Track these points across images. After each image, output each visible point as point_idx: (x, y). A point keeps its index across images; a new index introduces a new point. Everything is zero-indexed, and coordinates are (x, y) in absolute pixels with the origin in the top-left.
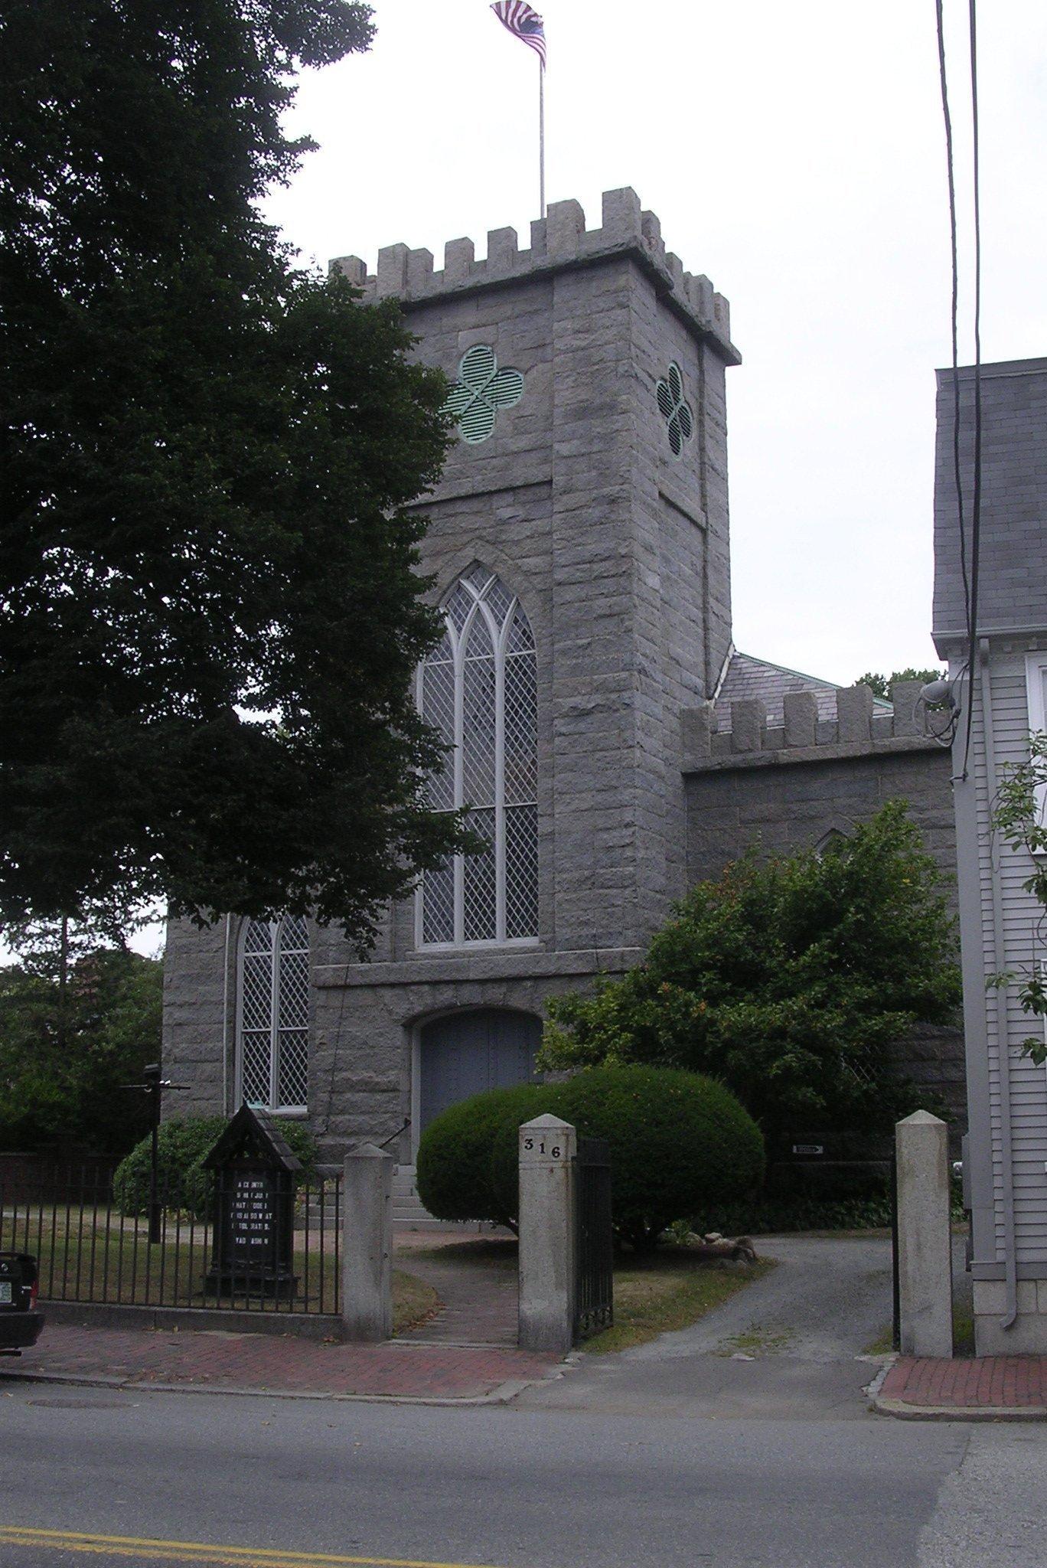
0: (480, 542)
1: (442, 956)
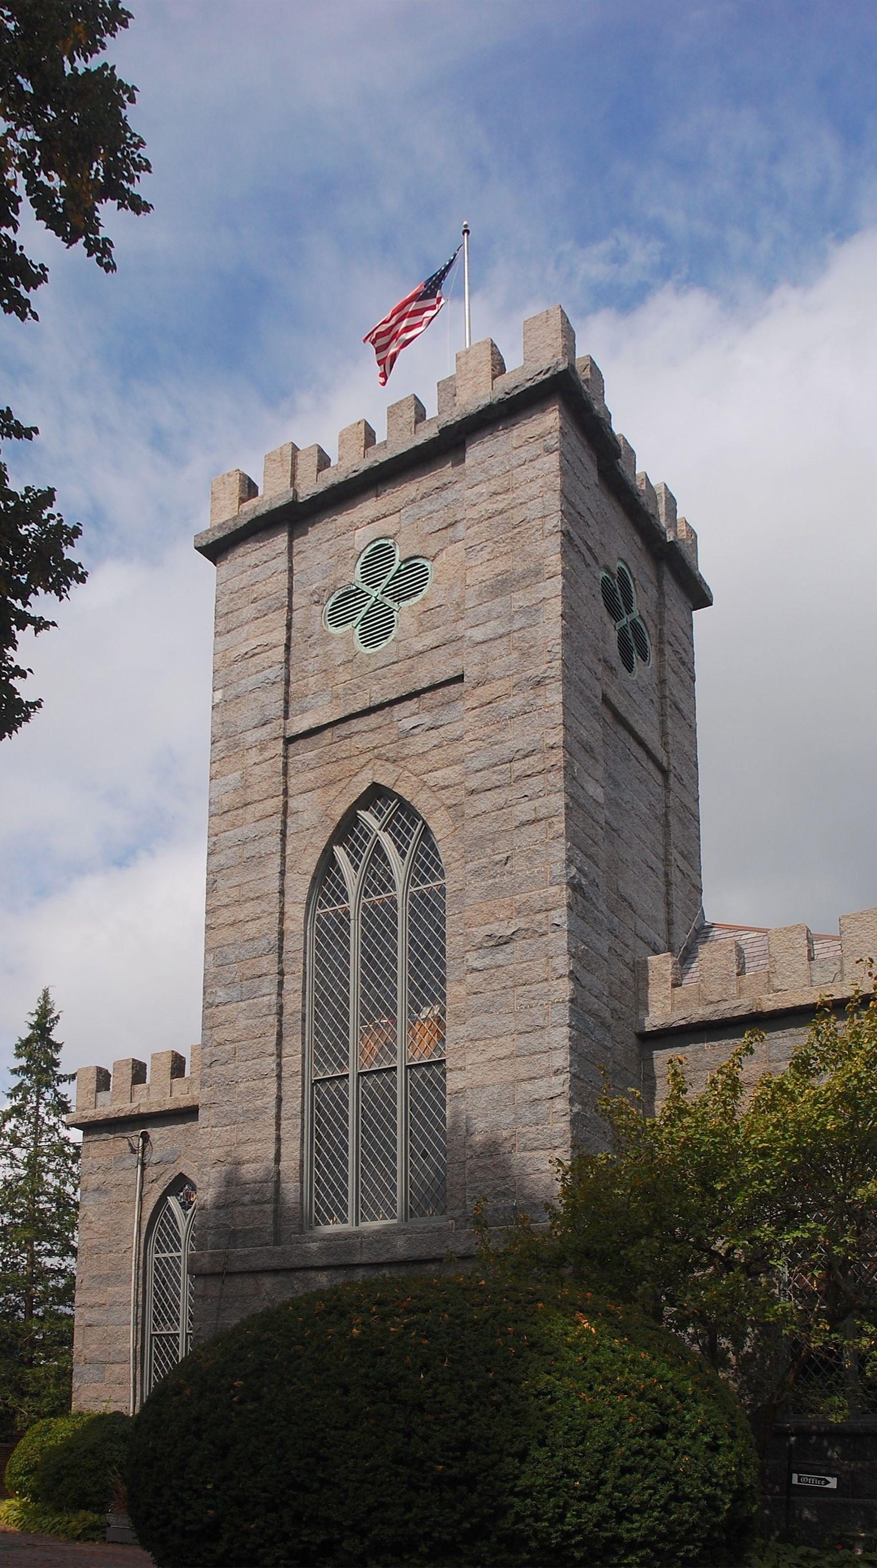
0: (379, 762)
1: (332, 1238)
